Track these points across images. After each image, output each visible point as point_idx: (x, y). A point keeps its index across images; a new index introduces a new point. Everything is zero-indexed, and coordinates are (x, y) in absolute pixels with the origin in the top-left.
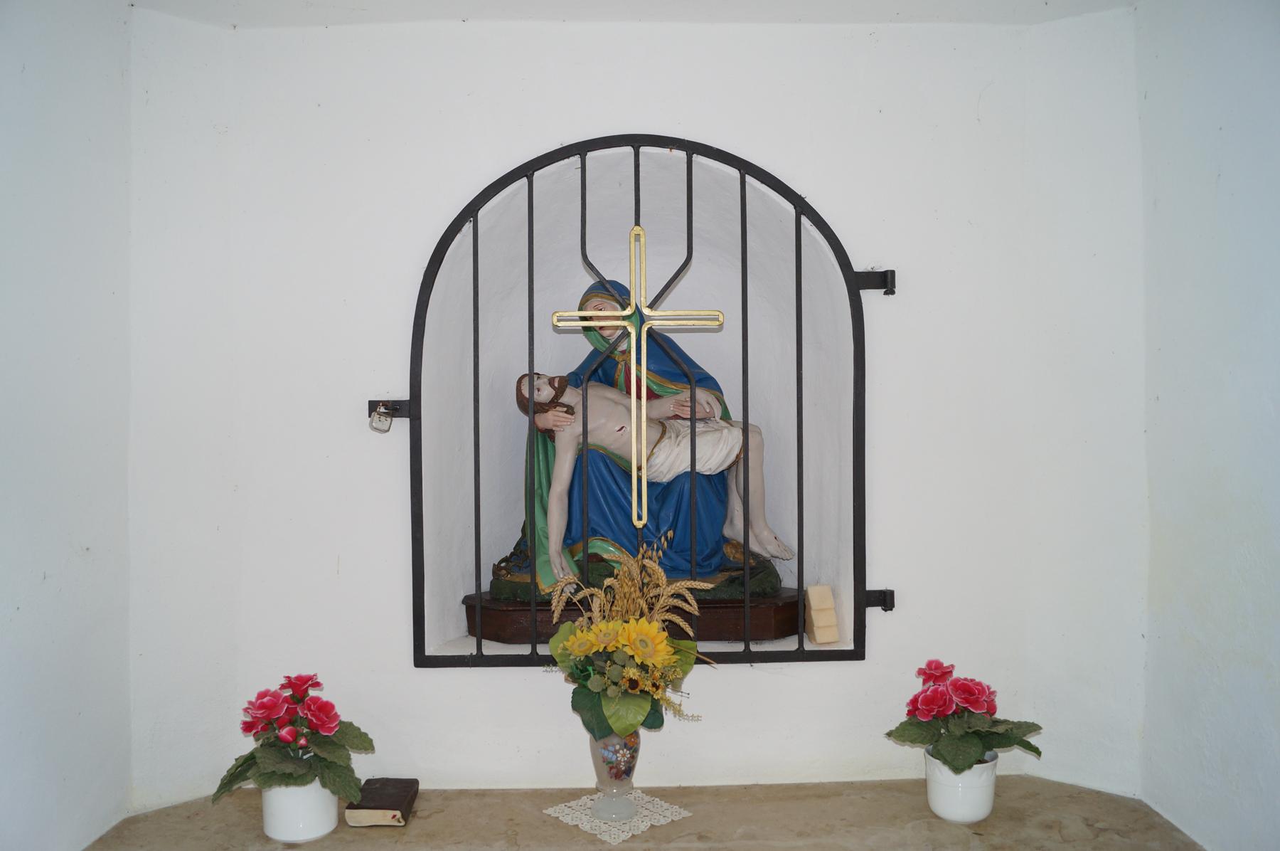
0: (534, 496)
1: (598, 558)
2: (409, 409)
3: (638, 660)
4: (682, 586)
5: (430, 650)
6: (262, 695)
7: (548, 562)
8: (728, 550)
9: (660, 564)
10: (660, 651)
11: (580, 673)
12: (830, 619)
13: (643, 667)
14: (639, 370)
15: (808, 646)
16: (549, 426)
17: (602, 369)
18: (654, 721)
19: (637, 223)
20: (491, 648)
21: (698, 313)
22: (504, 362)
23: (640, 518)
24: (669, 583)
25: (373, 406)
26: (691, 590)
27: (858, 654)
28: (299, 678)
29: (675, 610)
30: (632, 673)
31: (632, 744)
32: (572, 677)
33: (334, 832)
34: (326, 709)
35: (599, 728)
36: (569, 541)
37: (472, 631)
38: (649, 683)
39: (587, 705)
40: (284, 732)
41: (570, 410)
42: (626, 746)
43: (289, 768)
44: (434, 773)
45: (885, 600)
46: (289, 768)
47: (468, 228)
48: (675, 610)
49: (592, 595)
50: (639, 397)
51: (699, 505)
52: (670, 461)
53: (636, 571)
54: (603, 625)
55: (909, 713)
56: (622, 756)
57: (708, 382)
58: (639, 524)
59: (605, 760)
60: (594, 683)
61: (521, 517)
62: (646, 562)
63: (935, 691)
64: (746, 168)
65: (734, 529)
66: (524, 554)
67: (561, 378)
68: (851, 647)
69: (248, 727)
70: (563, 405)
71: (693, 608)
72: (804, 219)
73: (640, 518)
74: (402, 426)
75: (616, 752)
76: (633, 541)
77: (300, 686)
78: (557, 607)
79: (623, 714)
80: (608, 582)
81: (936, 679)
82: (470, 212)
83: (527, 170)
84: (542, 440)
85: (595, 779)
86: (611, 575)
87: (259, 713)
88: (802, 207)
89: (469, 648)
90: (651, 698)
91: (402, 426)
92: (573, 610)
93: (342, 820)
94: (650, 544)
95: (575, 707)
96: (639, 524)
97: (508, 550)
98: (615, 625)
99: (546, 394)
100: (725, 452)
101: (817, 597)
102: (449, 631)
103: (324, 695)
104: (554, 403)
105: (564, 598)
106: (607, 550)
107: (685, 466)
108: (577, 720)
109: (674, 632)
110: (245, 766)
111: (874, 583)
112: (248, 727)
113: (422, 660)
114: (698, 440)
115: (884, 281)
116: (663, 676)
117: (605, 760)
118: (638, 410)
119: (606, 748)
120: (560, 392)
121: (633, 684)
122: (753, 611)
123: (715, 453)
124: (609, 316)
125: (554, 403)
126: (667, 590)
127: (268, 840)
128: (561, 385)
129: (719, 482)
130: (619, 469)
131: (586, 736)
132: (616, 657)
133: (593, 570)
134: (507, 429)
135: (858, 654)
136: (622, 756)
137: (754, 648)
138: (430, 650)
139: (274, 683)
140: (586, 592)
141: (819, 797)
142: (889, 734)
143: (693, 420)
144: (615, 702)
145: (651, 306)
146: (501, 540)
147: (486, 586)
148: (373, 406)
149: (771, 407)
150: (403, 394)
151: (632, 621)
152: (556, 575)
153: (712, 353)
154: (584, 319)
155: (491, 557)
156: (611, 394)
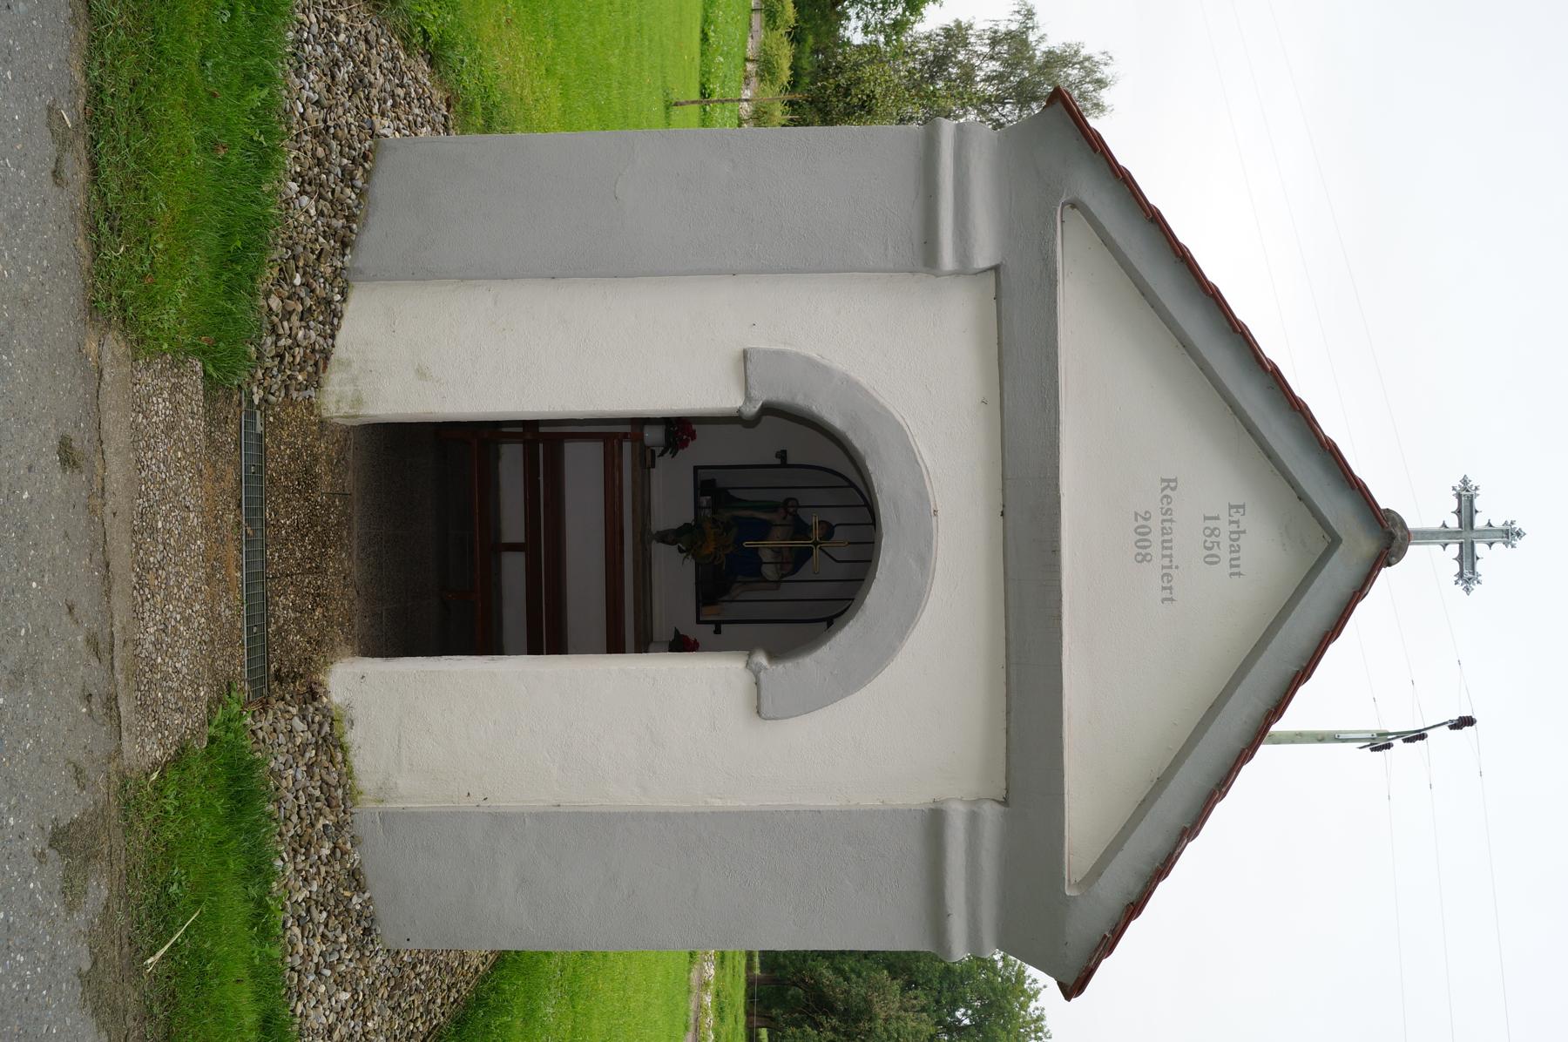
2: (784, 464)
12: (710, 613)
18: (681, 551)
21: (818, 564)
27: (698, 622)
51: (749, 566)
52: (766, 556)
57: (795, 571)
65: (740, 578)
84: (772, 507)
85: (662, 528)
90: (690, 550)
91: (778, 461)
123: (769, 571)
124: (816, 534)
129: (759, 573)
135: (698, 622)
137: (513, 527)
141: (108, 593)
142: (1465, 481)
149: (788, 590)
150: (790, 461)
153: (805, 572)
155: (732, 492)
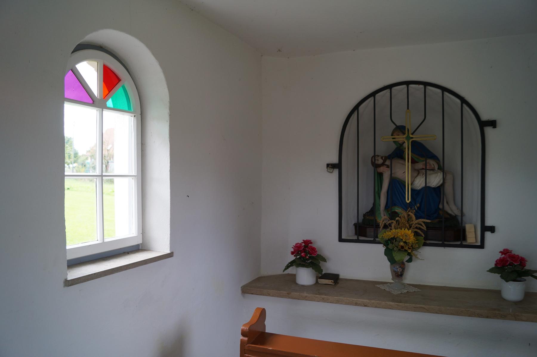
0: (377, 194)
1: (396, 213)
3: (404, 240)
4: (420, 221)
5: (343, 237)
6: (296, 244)
7: (380, 213)
8: (441, 212)
9: (415, 215)
10: (412, 239)
11: (386, 243)
13: (405, 242)
14: (408, 153)
15: (464, 243)
16: (381, 171)
17: (398, 154)
19: (408, 109)
20: (361, 238)
21: (431, 134)
22: (367, 150)
23: (408, 200)
24: (417, 219)
25: (328, 165)
26: (424, 222)
28: (307, 240)
29: (416, 228)
30: (402, 244)
31: (402, 266)
32: (385, 245)
33: (315, 284)
34: (314, 249)
35: (392, 261)
36: (387, 207)
37: (356, 234)
38: (407, 247)
39: (388, 253)
40: (303, 254)
41: (388, 166)
42: (400, 267)
43: (304, 263)
44: (343, 275)
45: (492, 229)
46: (304, 263)
47: (356, 113)
48: (416, 228)
49: (392, 223)
50: (408, 161)
52: (420, 183)
53: (406, 216)
54: (394, 230)
55: (495, 264)
56: (399, 270)
57: (434, 157)
58: (408, 202)
59: (395, 271)
60: (390, 246)
61: (372, 201)
62: (410, 213)
63: (504, 257)
64: (444, 89)
66: (373, 212)
67: (385, 157)
68: (479, 244)
69: (292, 253)
70: (386, 165)
71: (424, 228)
72: (464, 105)
73: (408, 200)
74: (336, 172)
75: (397, 269)
76: (406, 207)
77: (307, 243)
78: (381, 225)
79: (398, 257)
80: (397, 218)
81: (505, 254)
82: (356, 108)
83: (373, 94)
86: (398, 216)
87: (296, 248)
88: (463, 101)
89: (355, 238)
91: (336, 172)
92: (386, 227)
93: (317, 282)
94: (411, 208)
95: (385, 254)
96: (408, 202)
97: (369, 209)
98: (399, 230)
99: (380, 161)
100: (439, 180)
101: (469, 229)
102: (349, 232)
103: (313, 245)
104: (383, 164)
105: (384, 223)
106: (398, 210)
107: (423, 185)
108: (386, 258)
109: (416, 234)
110: (291, 264)
111: (488, 223)
112: (292, 253)
113: (341, 240)
114: (118, 108)
115: (493, 124)
116: (412, 246)
117: (395, 271)
118: (408, 165)
119: (394, 267)
120: (385, 161)
121: (402, 247)
122: (448, 231)
123: (435, 180)
124: (401, 138)
125: (383, 164)
126: (415, 222)
127: (297, 284)
128: (385, 159)
130: (402, 184)
131: (389, 263)
132: (398, 239)
133: (393, 215)
134: (367, 171)
136: (399, 270)
138: (343, 237)
139: (300, 241)
140: (390, 221)
143: (426, 169)
144: (399, 255)
145: (412, 134)
146: (366, 205)
147: (361, 220)
148: (328, 165)
151: (403, 229)
152: (382, 218)
154: (393, 138)
155: (363, 211)
156: (401, 161)
